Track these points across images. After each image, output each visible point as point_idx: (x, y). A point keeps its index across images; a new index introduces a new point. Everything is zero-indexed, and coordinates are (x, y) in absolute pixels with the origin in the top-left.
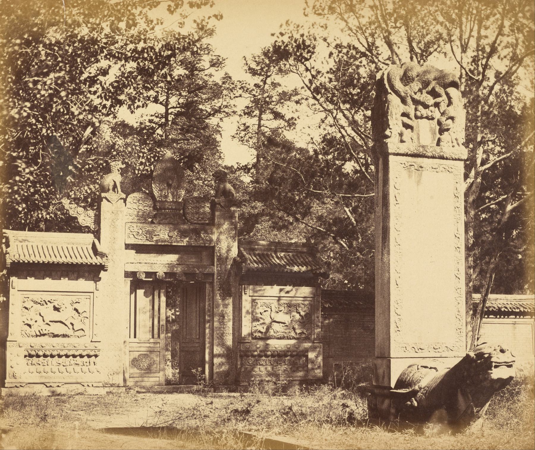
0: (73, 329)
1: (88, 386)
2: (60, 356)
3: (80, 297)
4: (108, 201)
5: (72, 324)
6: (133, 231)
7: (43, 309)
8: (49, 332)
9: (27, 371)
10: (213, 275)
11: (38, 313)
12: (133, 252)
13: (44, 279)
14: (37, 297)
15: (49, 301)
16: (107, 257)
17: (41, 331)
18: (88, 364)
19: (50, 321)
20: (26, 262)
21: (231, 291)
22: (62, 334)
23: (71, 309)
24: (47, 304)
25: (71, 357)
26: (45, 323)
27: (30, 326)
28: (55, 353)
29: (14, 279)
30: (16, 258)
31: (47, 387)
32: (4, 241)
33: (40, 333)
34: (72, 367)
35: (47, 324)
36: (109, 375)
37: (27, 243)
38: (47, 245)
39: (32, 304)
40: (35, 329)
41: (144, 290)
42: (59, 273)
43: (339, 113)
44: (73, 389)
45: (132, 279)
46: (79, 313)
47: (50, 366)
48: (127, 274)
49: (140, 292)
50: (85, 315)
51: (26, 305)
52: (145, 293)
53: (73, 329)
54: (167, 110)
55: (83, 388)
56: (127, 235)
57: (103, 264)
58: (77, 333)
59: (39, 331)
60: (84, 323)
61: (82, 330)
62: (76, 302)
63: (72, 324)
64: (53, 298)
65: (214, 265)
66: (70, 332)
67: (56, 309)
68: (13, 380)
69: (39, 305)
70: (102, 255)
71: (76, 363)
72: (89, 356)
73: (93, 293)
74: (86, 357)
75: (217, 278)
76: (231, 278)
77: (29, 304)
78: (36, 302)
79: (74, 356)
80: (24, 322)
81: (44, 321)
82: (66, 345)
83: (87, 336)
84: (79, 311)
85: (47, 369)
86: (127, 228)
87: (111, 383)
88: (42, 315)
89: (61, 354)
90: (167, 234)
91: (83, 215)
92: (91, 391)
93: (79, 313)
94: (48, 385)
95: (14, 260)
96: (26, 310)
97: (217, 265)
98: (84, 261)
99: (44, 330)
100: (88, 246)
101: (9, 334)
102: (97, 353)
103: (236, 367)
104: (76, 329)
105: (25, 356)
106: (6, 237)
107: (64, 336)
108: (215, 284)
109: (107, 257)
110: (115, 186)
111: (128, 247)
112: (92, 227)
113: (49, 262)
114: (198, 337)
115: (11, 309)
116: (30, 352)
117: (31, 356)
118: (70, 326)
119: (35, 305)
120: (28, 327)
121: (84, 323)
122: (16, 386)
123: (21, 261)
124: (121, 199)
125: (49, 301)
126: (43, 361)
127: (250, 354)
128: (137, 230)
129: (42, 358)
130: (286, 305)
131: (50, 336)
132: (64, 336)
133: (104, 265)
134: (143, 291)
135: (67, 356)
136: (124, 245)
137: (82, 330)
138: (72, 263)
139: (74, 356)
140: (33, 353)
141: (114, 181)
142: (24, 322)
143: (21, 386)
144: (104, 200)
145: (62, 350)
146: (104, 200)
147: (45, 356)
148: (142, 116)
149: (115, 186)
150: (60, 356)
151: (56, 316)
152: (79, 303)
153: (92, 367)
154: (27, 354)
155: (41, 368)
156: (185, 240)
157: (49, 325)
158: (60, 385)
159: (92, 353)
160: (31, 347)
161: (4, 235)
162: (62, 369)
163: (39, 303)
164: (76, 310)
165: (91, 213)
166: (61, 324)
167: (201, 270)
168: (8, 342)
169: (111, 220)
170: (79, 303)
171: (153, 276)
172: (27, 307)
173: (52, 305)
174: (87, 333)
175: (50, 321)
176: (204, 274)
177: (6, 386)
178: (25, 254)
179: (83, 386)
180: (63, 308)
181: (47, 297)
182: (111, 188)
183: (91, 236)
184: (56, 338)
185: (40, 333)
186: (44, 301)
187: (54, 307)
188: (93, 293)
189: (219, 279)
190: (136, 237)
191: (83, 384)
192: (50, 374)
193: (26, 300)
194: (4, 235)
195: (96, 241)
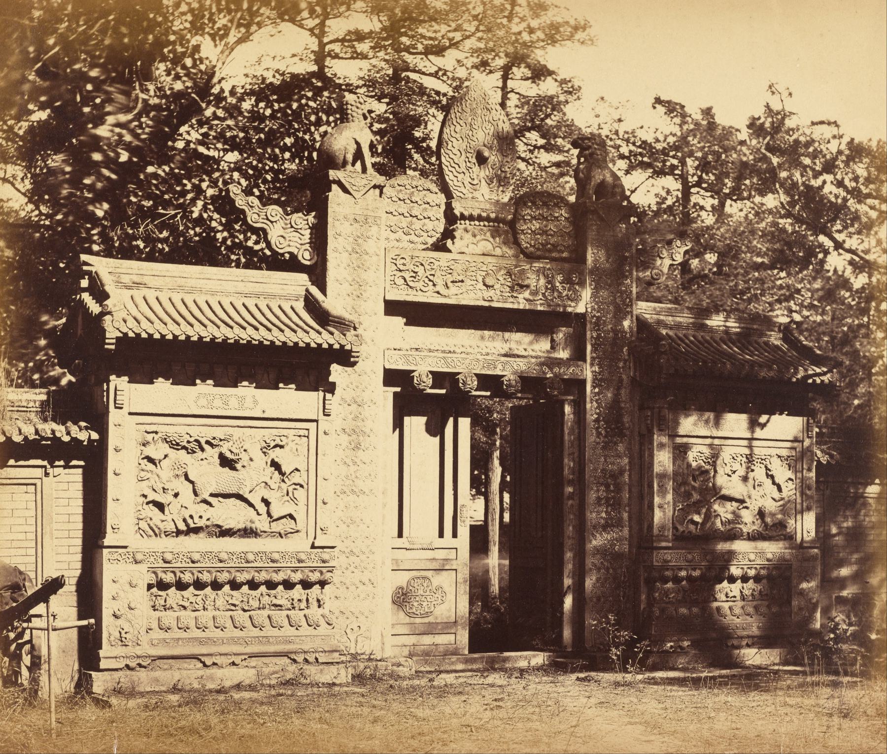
0: (269, 514)
1: (306, 660)
3: (285, 432)
4: (345, 190)
6: (402, 267)
7: (195, 466)
8: (208, 523)
9: (155, 625)
10: (584, 382)
14: (179, 430)
15: (207, 442)
17: (190, 521)
18: (303, 605)
19: (212, 495)
20: (157, 336)
21: (623, 424)
23: (261, 461)
24: (203, 450)
25: (263, 588)
26: (199, 499)
27: (160, 507)
28: (223, 577)
29: (118, 383)
30: (131, 328)
31: (205, 665)
32: (84, 283)
33: (187, 525)
34: (265, 613)
35: (205, 502)
36: (348, 631)
39: (165, 449)
40: (174, 516)
41: (424, 419)
44: (271, 669)
45: (398, 389)
47: (210, 613)
48: (391, 377)
49: (415, 424)
50: (296, 478)
51: (150, 451)
52: (427, 424)
53: (269, 514)
54: (322, 45)
55: (293, 668)
56: (388, 278)
57: (348, 347)
58: (277, 527)
59: (185, 520)
60: (294, 500)
61: (291, 516)
62: (276, 446)
64: (219, 433)
65: (585, 361)
66: (261, 523)
67: (227, 462)
68: (120, 651)
70: (343, 325)
71: (275, 601)
72: (307, 585)
74: (299, 587)
76: (623, 392)
77: (157, 451)
78: (175, 445)
79: (271, 585)
80: (145, 496)
81: (196, 494)
82: (251, 557)
84: (284, 469)
85: (206, 617)
86: (388, 260)
87: (353, 651)
88: (191, 478)
90: (480, 279)
91: (281, 223)
94: (209, 662)
95: (125, 330)
96: (150, 466)
97: (593, 359)
99: (196, 519)
101: (109, 529)
102: (328, 576)
105: (150, 587)
106: (89, 273)
107: (248, 532)
108: (588, 406)
109: (355, 329)
110: (358, 155)
111: (393, 308)
112: (305, 257)
113: (213, 339)
115: (113, 462)
117: (162, 586)
118: (262, 508)
119: (172, 453)
121: (294, 500)
122: (127, 666)
123: (144, 335)
124: (375, 187)
125: (207, 442)
126: (192, 599)
128: (412, 267)
131: (210, 535)
132: (248, 532)
133: (351, 351)
137: (291, 516)
139: (271, 585)
140: (169, 578)
141: (357, 143)
142: (145, 496)
143: (140, 665)
144: (335, 187)
145: (240, 570)
146: (335, 187)
147: (199, 585)
148: (259, 62)
149: (358, 155)
150: (235, 585)
151: (225, 480)
152: (282, 447)
154: (154, 582)
155: (187, 617)
156: (521, 296)
157: (210, 504)
158: (237, 660)
159: (315, 577)
160: (165, 562)
161: (85, 268)
162: (242, 617)
163: (184, 448)
164: (275, 465)
165: (303, 221)
166: (238, 502)
167: (556, 370)
168: (105, 551)
169: (351, 239)
170: (282, 447)
173: (217, 451)
174: (301, 525)
175: (212, 495)
177: (103, 664)
178: (148, 316)
179: (294, 661)
180: (244, 457)
181: (202, 431)
182: (350, 157)
183: (303, 278)
184: (227, 539)
185: (187, 525)
186: (196, 441)
187: (222, 457)
188: (316, 421)
190: (411, 284)
191: (293, 656)
193: (149, 437)
194: (85, 268)
195: (315, 291)
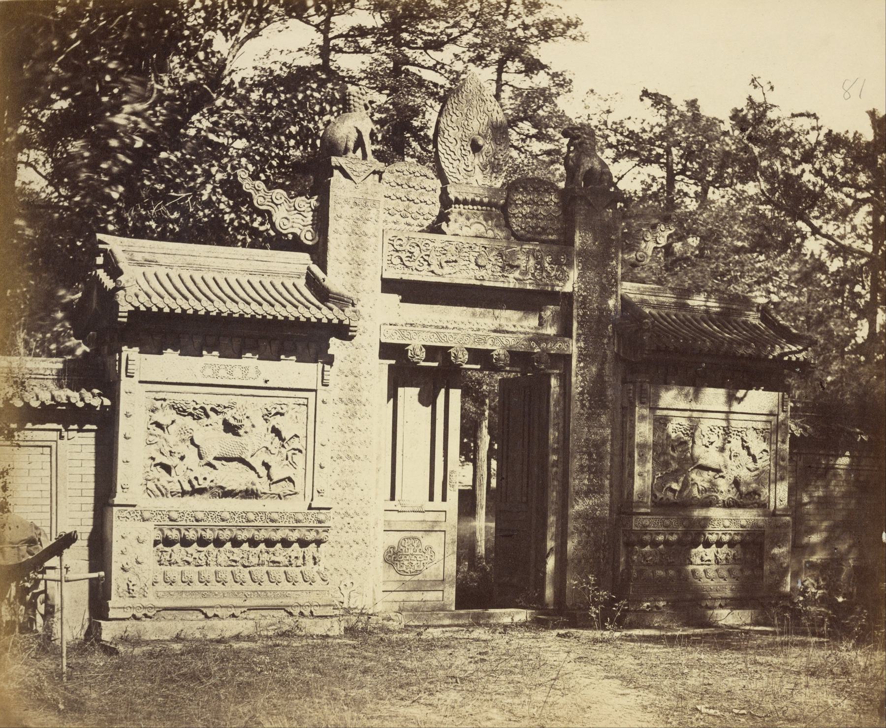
0: (269, 477)
1: (301, 614)
2: (236, 543)
4: (346, 175)
5: (267, 466)
6: (398, 248)
8: (212, 484)
9: (160, 578)
11: (187, 437)
12: (396, 298)
13: (161, 353)
14: (187, 397)
15: (212, 409)
16: (353, 305)
17: (195, 483)
18: (300, 561)
19: (216, 459)
21: (606, 396)
22: (243, 488)
23: (262, 427)
24: (208, 416)
26: (203, 462)
27: (167, 469)
29: (130, 353)
31: (207, 617)
32: (100, 260)
33: (192, 486)
36: (342, 587)
37: (155, 268)
38: (225, 275)
39: (173, 415)
41: (417, 390)
42: (198, 341)
43: (336, 33)
45: (393, 362)
46: (282, 439)
47: (213, 568)
48: (387, 350)
49: (409, 395)
51: (158, 417)
53: (269, 477)
55: (289, 620)
56: (386, 258)
57: (346, 322)
59: (190, 482)
60: (293, 464)
61: (290, 479)
63: (267, 466)
64: (224, 401)
65: (571, 337)
66: (262, 486)
67: (231, 428)
68: (129, 602)
69: (190, 417)
70: (342, 301)
71: (273, 558)
73: (316, 391)
74: (296, 545)
75: (577, 367)
76: (607, 366)
78: (181, 412)
79: (270, 543)
80: (153, 459)
82: (251, 517)
83: (301, 496)
84: (284, 435)
85: (208, 572)
86: (386, 241)
88: (197, 442)
89: (240, 538)
90: (473, 260)
92: (311, 627)
93: (282, 439)
95: (137, 304)
96: (159, 431)
97: (579, 335)
98: (291, 313)
99: (201, 481)
100: (297, 282)
101: (119, 489)
102: (323, 535)
103: (615, 568)
104: (275, 479)
105: (156, 543)
106: (105, 251)
107: (250, 494)
108: (574, 379)
109: (353, 305)
110: (359, 143)
111: (389, 286)
112: (308, 237)
114: (524, 499)
115: (124, 426)
116: (167, 532)
117: (168, 542)
118: (262, 471)
119: (179, 419)
120: (163, 472)
121: (293, 464)
122: (134, 616)
123: (155, 309)
124: (374, 172)
125: (212, 409)
126: (196, 555)
127: (647, 538)
128: (408, 248)
129: (178, 546)
130: (722, 431)
132: (250, 494)
133: (349, 326)
134: (415, 391)
135: (253, 543)
136: (380, 283)
137: (290, 479)
138: (275, 317)
140: (174, 535)
141: (359, 131)
142: (153, 459)
143: (146, 616)
144: (336, 172)
145: (241, 528)
146: (336, 172)
147: (202, 542)
151: (228, 444)
153: (309, 567)
155: (191, 571)
156: (511, 276)
158: (237, 612)
159: (311, 536)
161: (101, 246)
163: (190, 414)
164: (276, 431)
165: (306, 204)
166: (240, 465)
169: (351, 221)
170: (282, 414)
171: (440, 357)
172: (161, 422)
174: (299, 488)
175: (216, 459)
176: (550, 355)
177: (112, 614)
179: (291, 614)
180: (247, 423)
181: (208, 399)
182: (351, 145)
183: (305, 258)
184: (229, 499)
185: (192, 486)
187: (226, 423)
188: (316, 391)
189: (582, 368)
190: (407, 263)
191: (289, 609)
192: (267, 586)
193: (158, 404)
194: (101, 246)
195: (316, 269)
